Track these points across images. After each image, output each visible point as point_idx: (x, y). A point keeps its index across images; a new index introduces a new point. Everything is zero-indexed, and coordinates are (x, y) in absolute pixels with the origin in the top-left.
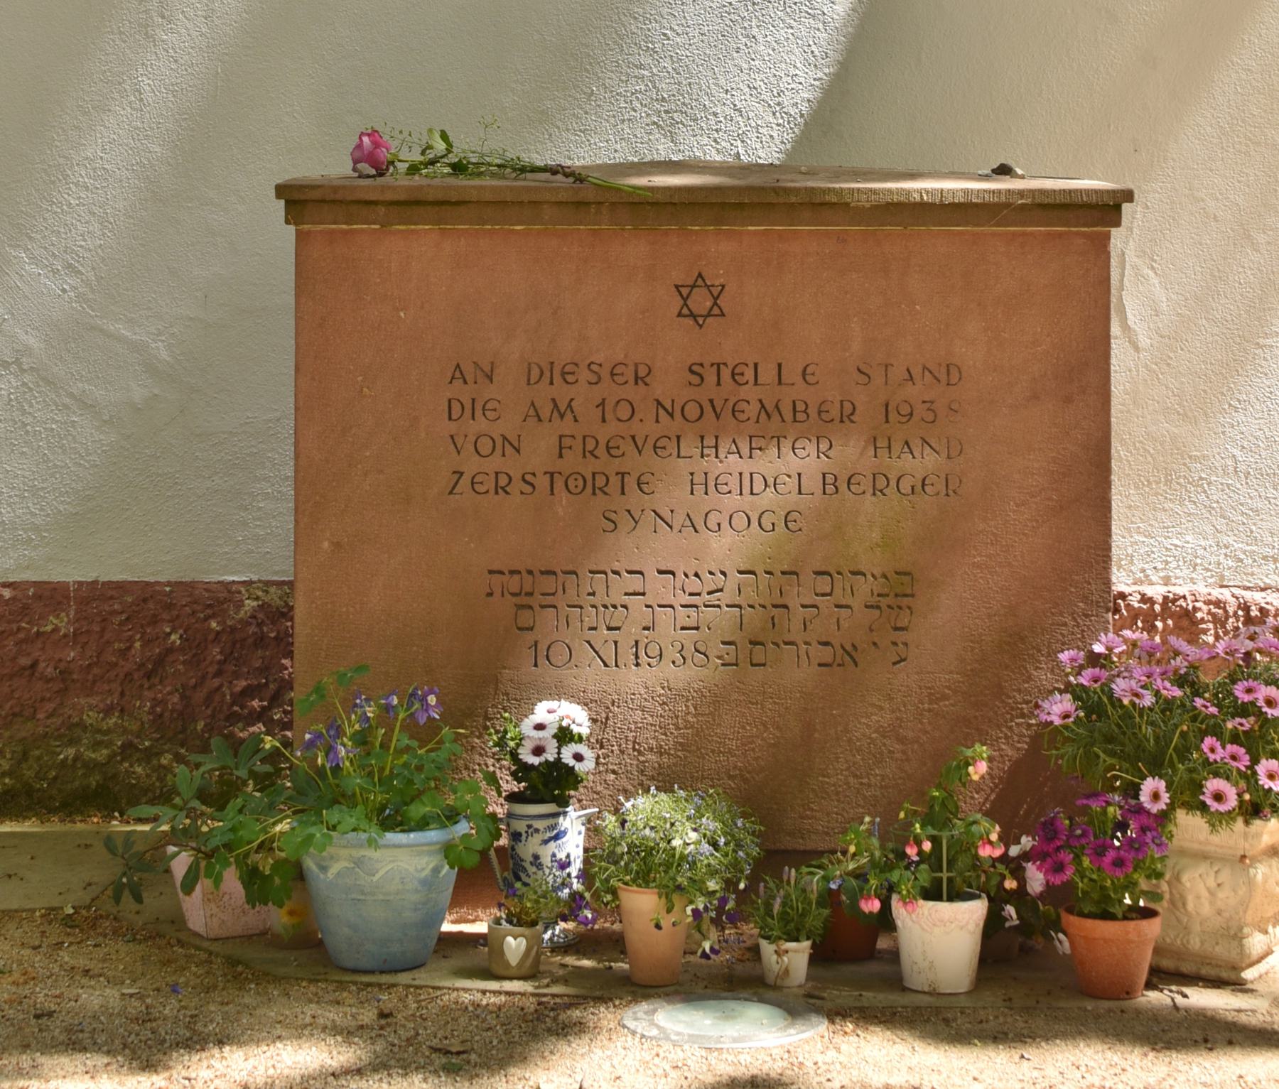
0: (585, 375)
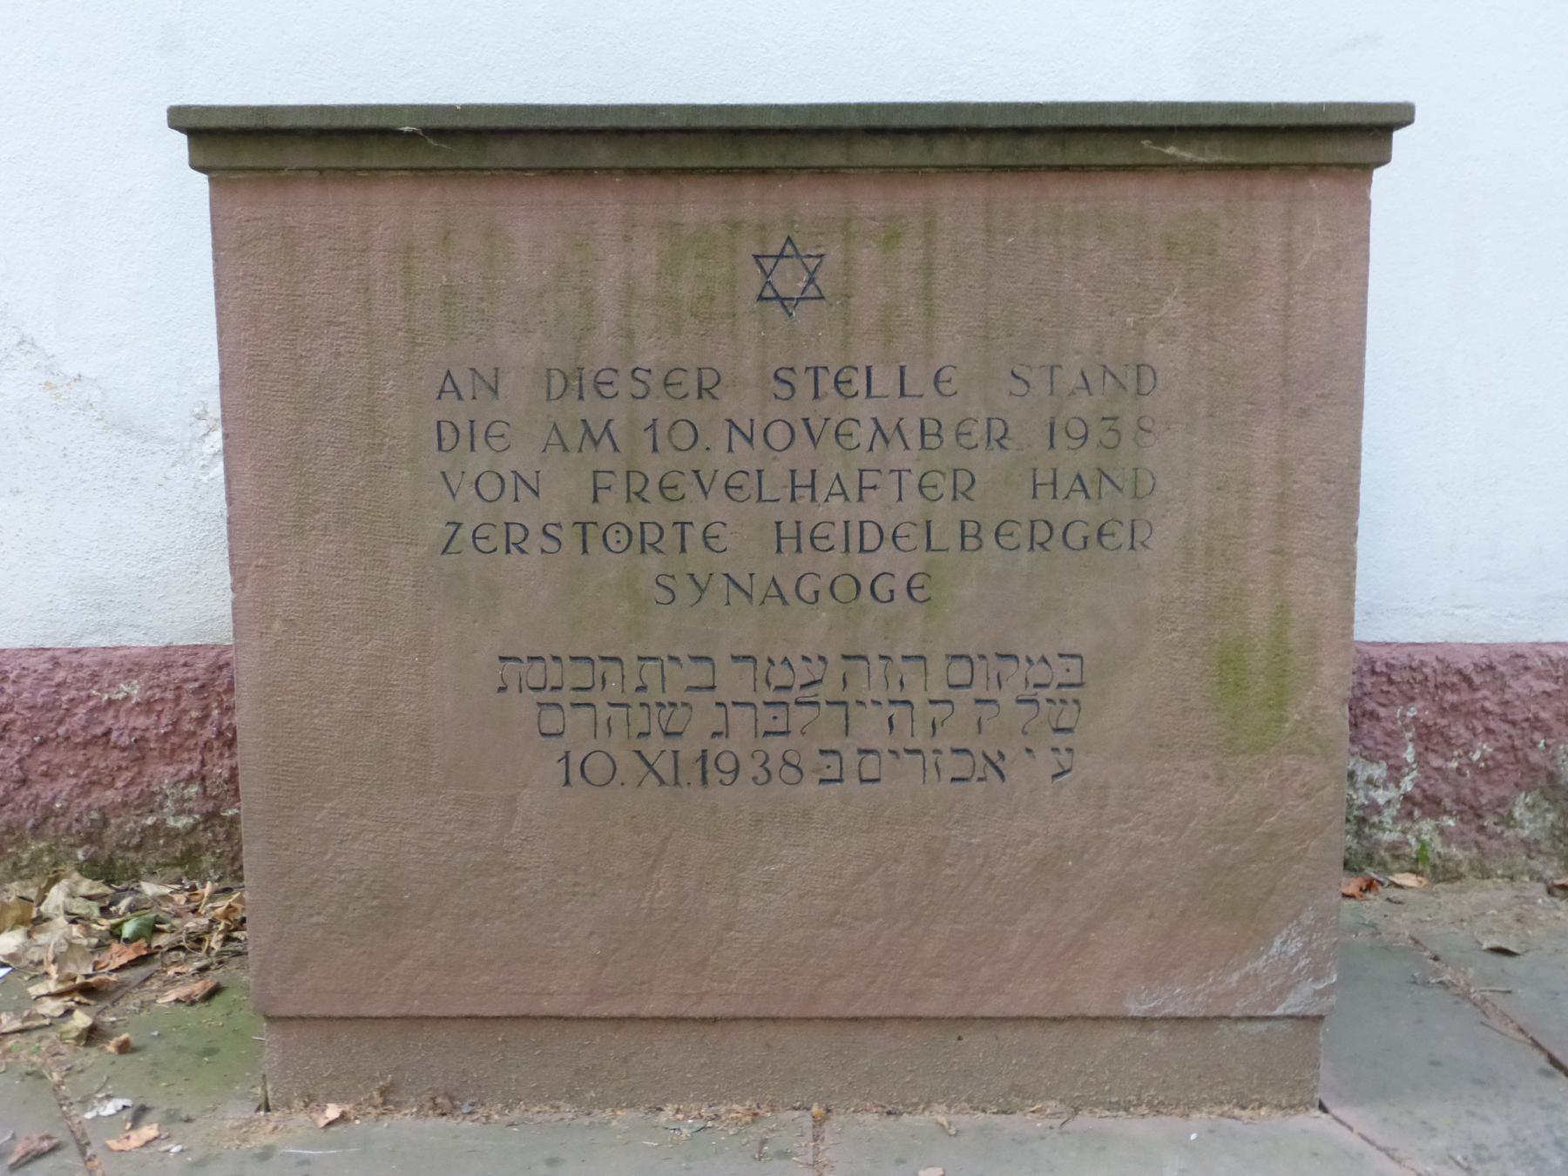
0: (625, 385)
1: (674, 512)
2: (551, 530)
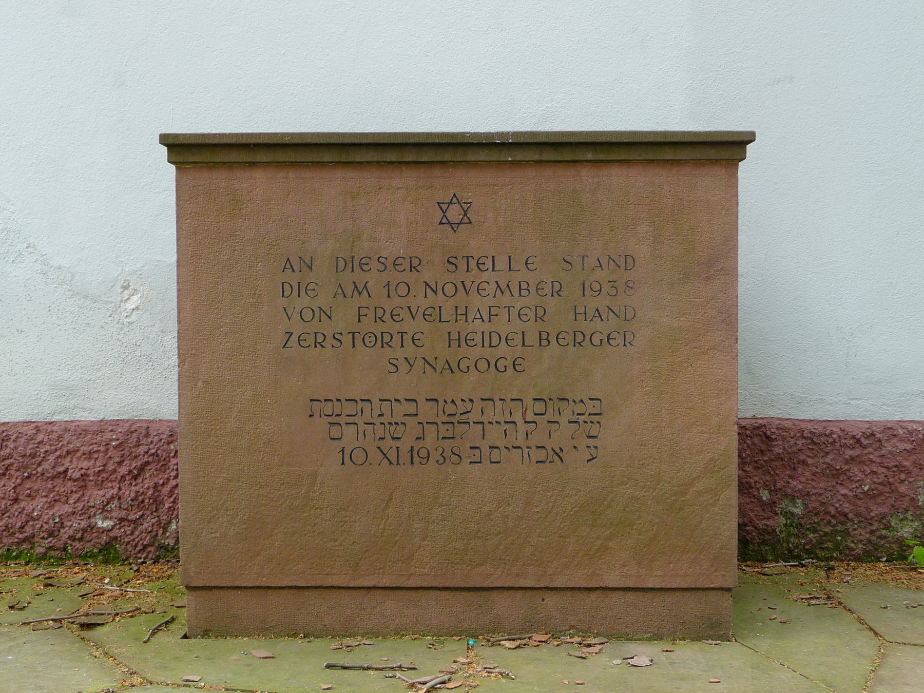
1: (397, 327)
2: (337, 336)
